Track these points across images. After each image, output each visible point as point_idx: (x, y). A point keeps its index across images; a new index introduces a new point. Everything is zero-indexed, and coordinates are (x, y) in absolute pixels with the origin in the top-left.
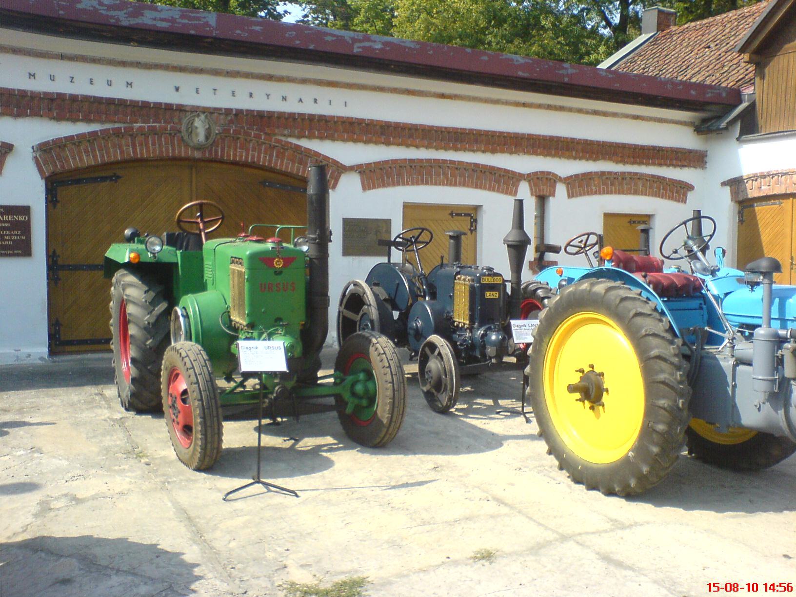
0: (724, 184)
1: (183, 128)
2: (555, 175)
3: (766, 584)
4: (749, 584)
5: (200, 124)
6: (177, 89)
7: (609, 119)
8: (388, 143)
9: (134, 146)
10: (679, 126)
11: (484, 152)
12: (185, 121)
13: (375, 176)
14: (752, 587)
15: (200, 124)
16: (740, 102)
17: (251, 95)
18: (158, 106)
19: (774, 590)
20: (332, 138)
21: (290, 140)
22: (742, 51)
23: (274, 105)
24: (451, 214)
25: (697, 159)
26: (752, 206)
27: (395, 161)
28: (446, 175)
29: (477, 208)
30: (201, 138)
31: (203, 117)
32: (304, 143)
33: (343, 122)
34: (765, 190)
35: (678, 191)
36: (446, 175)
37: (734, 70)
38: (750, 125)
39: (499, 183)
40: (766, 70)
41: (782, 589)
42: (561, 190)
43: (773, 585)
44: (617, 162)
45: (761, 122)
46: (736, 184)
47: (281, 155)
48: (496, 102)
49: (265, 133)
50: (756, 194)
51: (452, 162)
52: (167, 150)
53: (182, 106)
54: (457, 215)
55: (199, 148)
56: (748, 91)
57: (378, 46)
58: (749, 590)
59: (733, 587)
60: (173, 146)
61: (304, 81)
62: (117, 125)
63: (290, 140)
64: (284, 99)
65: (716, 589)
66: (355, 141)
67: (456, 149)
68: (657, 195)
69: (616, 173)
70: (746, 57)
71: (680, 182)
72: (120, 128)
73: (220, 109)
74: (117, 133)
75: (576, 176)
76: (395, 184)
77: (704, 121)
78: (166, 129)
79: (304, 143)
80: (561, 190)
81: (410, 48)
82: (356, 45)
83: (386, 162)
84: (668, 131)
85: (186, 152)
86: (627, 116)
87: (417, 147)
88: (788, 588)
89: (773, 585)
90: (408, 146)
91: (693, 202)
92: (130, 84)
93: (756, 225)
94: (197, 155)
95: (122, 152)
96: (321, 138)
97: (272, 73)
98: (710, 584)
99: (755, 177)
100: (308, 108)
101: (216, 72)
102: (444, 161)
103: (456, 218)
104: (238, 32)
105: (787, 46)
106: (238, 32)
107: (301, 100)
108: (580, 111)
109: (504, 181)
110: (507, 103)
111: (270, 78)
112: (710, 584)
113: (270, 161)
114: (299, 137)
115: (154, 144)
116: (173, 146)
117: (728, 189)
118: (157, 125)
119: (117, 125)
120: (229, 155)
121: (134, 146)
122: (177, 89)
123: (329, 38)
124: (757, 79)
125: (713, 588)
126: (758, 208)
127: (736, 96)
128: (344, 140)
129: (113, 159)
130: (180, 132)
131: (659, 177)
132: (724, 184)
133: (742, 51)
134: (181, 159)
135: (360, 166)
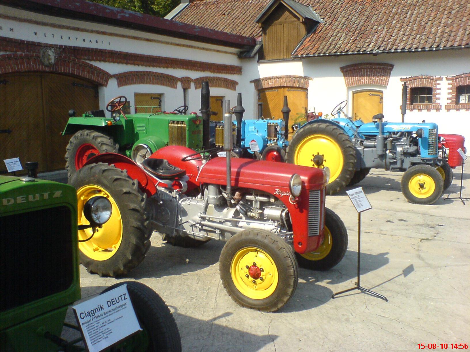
0: (251, 82)
1: (41, 55)
2: (190, 78)
3: (452, 344)
4: (442, 345)
5: (51, 53)
6: (36, 34)
7: (208, 52)
8: (127, 63)
9: (17, 65)
10: (232, 55)
11: (164, 67)
12: (42, 52)
13: (124, 79)
14: (444, 346)
15: (51, 53)
16: (255, 44)
17: (69, 38)
18: (28, 42)
19: (457, 348)
20: (105, 61)
21: (87, 62)
22: (258, 22)
23: (79, 44)
24: (151, 98)
25: (237, 70)
26: (264, 92)
27: (131, 72)
28: (150, 79)
29: (161, 95)
30: (52, 61)
31: (53, 50)
32: (93, 63)
33: (109, 53)
34: (271, 84)
35: (232, 85)
36: (150, 79)
37: (249, 29)
38: (261, 57)
39: (170, 82)
40: (267, 31)
41: (462, 347)
42: (192, 85)
43: (457, 345)
44: (211, 72)
45: (266, 54)
46: (257, 82)
47: (84, 70)
48: (167, 43)
49: (77, 59)
50: (267, 86)
51: (153, 73)
52: (33, 68)
53: (40, 43)
54: (154, 98)
55: (49, 66)
56: (259, 39)
57: (127, 16)
58: (442, 348)
59: (433, 346)
60: (36, 65)
61: (92, 31)
62: (8, 53)
63: (87, 62)
64: (11, 30)
65: (423, 347)
66: (114, 62)
67: (153, 66)
68: (225, 87)
69: (212, 77)
70: (260, 25)
71: (234, 81)
72: (10, 54)
73: (57, 45)
74: (9, 57)
75: (198, 79)
76: (131, 83)
77: (241, 53)
78: (33, 55)
79: (93, 63)
80: (192, 85)
81: (139, 17)
82: (119, 14)
83: (127, 73)
84: (226, 57)
85: (42, 68)
86: (214, 50)
87: (138, 65)
88: (465, 346)
89: (457, 345)
90: (135, 65)
91: (239, 89)
92: (11, 30)
93: (267, 101)
94: (47, 70)
95: (12, 68)
96: (100, 61)
97: (107, 31)
98: (419, 344)
99: (266, 79)
100: (93, 46)
101: (54, 26)
102: (150, 72)
103: (154, 100)
104: (70, 5)
105: (275, 22)
106: (70, 5)
107: (91, 41)
108: (198, 48)
109: (171, 81)
110: (184, 46)
111: (78, 29)
112: (419, 344)
113: (79, 73)
114: (90, 60)
115: (27, 64)
116: (36, 65)
117: (253, 84)
118: (23, 53)
119: (8, 53)
120: (61, 70)
121: (17, 65)
122: (36, 34)
123: (108, 11)
124: (263, 35)
125: (421, 347)
126: (267, 93)
127: (254, 42)
128: (109, 62)
129: (7, 71)
130: (39, 57)
131: (227, 79)
132: (251, 82)
133: (258, 22)
134: (34, 72)
135: (117, 75)
